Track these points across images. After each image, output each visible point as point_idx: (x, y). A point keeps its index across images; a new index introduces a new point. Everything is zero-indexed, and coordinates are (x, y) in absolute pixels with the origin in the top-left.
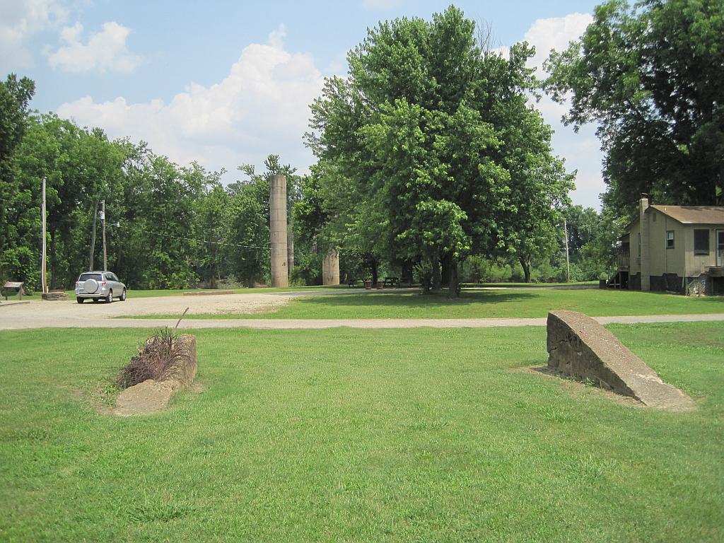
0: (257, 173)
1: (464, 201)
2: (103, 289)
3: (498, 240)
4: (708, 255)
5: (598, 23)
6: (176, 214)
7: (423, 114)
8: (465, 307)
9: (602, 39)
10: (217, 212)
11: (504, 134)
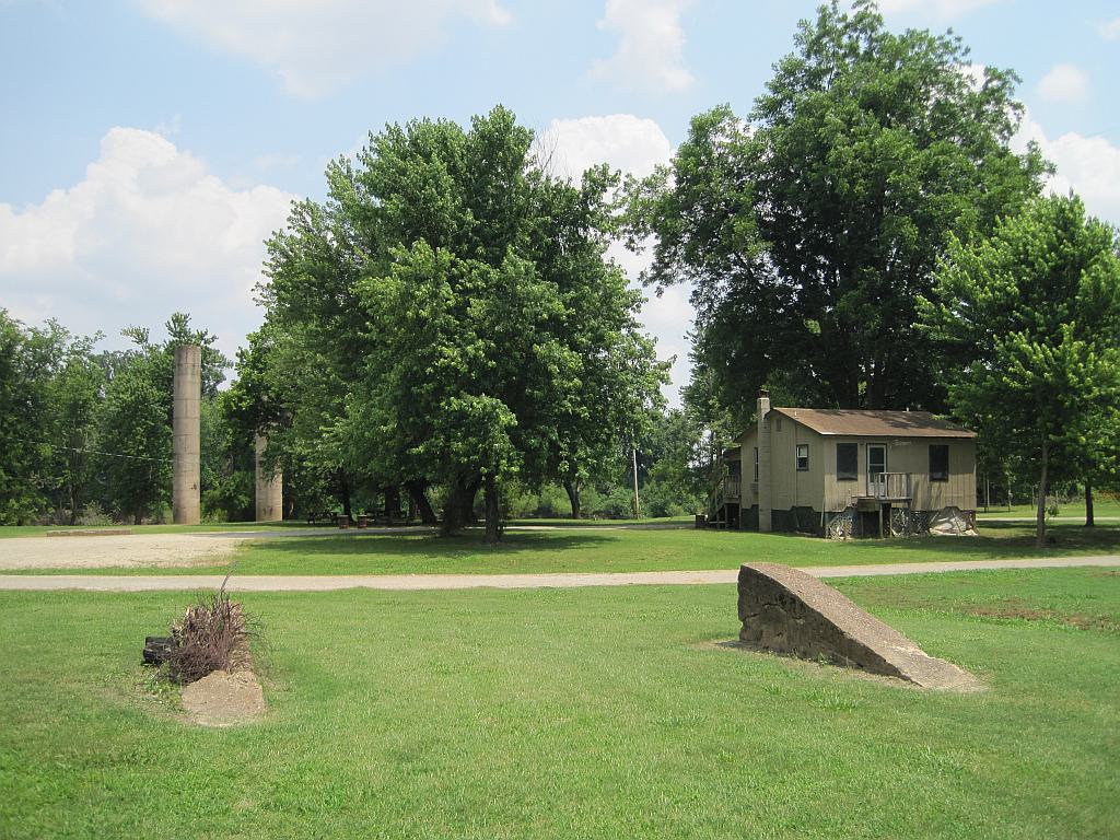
0: (152, 342)
1: (514, 401)
3: (561, 459)
4: (856, 480)
5: (697, 142)
7: (454, 264)
9: (702, 163)
10: (85, 402)
11: (573, 298)
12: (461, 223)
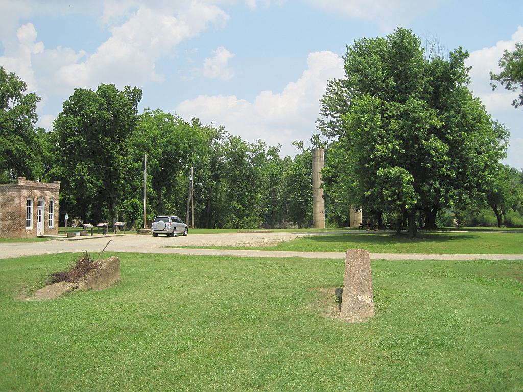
0: (305, 147)
1: (413, 168)
2: (169, 227)
3: (441, 196)
6: (247, 176)
7: (383, 104)
8: (415, 244)
12: (387, 85)
